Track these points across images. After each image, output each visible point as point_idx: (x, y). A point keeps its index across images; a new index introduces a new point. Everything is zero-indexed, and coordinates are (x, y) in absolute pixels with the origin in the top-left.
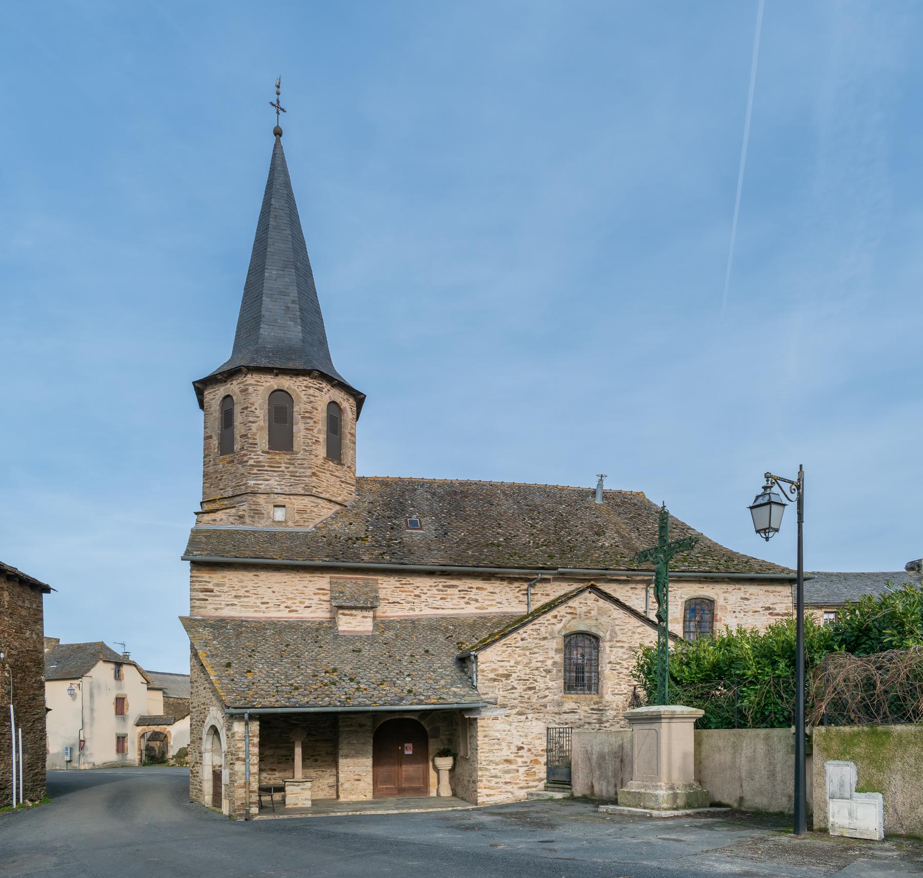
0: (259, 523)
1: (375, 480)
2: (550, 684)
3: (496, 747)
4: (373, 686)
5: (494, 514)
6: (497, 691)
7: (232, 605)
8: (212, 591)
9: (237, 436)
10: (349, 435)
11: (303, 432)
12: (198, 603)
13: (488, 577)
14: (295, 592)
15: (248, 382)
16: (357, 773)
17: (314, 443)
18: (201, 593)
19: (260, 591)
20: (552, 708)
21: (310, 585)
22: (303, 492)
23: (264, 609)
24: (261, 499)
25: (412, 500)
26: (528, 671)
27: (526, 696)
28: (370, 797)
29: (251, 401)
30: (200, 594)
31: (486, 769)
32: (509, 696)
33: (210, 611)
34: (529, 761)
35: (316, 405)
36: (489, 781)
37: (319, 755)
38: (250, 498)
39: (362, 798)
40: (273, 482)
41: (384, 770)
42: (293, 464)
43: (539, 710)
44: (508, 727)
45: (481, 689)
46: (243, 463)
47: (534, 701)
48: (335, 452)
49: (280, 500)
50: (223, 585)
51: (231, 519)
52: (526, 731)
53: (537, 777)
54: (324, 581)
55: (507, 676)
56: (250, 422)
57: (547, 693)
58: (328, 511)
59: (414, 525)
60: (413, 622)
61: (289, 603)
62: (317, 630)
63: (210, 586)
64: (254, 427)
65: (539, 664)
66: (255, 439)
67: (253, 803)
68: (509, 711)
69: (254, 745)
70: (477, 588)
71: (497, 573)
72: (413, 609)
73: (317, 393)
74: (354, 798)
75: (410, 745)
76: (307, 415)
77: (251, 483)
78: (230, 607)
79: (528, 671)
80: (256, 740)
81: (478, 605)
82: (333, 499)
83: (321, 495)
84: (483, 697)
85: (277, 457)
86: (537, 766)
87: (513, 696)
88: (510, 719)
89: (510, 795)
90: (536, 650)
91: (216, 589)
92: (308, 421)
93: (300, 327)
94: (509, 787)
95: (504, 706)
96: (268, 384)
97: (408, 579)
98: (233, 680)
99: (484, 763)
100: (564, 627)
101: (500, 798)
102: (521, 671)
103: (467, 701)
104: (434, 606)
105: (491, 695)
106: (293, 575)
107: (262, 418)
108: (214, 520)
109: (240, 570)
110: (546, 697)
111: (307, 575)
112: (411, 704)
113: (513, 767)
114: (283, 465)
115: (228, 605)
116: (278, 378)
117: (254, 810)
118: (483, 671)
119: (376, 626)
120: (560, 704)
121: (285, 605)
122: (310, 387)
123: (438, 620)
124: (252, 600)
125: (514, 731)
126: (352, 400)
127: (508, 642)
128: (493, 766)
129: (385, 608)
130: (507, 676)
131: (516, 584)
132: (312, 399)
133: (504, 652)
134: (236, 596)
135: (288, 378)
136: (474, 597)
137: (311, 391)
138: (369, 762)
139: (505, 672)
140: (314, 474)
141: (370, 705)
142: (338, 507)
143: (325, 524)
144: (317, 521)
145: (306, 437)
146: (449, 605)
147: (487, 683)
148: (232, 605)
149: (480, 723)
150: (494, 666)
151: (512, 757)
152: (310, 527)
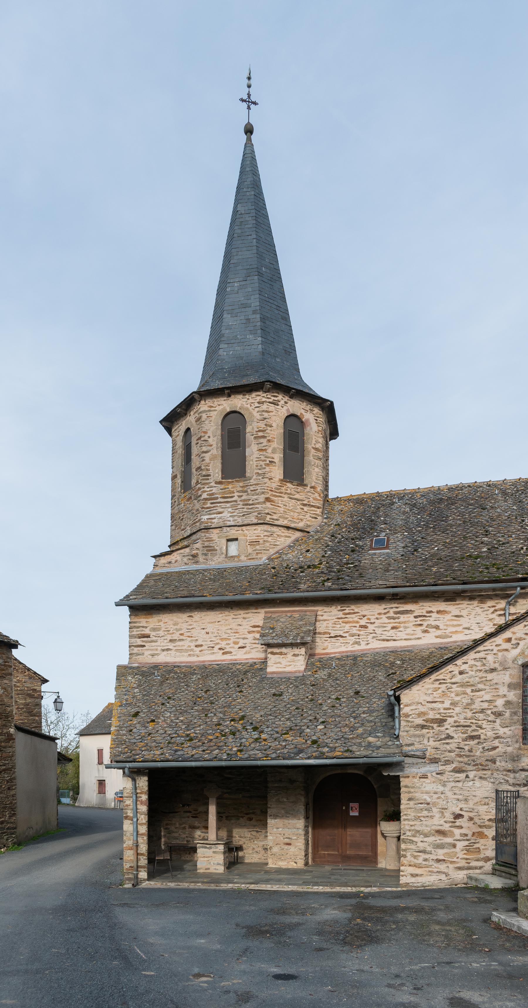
0: (212, 560)
1: (349, 499)
2: (502, 731)
3: (425, 813)
4: (276, 735)
5: (483, 519)
6: (425, 742)
7: (168, 650)
8: (148, 636)
9: (194, 470)
10: (313, 451)
11: (256, 454)
12: (136, 650)
13: (451, 597)
14: (229, 631)
15: (201, 409)
16: (286, 835)
17: (267, 465)
18: (139, 639)
19: (194, 633)
20: (503, 764)
21: (245, 623)
22: (255, 521)
23: (198, 652)
24: (214, 534)
25: (386, 516)
26: (469, 714)
27: (467, 748)
28: (300, 864)
29: (204, 430)
30: (138, 640)
31: (412, 842)
32: (443, 747)
33: (147, 658)
34: (470, 833)
35: (270, 422)
36: (415, 857)
37: (254, 813)
38: (203, 535)
39: (292, 865)
40: (226, 515)
41: (326, 834)
42: (246, 492)
43: (485, 766)
44: (441, 788)
45: (405, 739)
46: (198, 497)
47: (478, 754)
48: (294, 472)
49: (233, 532)
50: (159, 629)
51: (185, 560)
52: (466, 793)
53: (482, 856)
54: (257, 617)
55: (441, 722)
56: (204, 452)
57: (496, 743)
58: (284, 539)
59: (381, 544)
60: (355, 658)
61: (223, 644)
62: (245, 673)
63: (147, 631)
64: (207, 456)
65: (485, 705)
66: (208, 470)
67: (142, 867)
68: (441, 768)
69: (142, 803)
70: (438, 612)
71: (464, 591)
72: (358, 643)
73: (272, 407)
74: (283, 864)
75: (355, 805)
76: (260, 434)
77: (205, 518)
78: (165, 653)
79: (469, 714)
80: (144, 797)
81: (439, 633)
82: (293, 525)
83: (276, 523)
84: (406, 749)
85: (230, 486)
86: (482, 841)
87: (448, 747)
88: (444, 778)
89: (443, 877)
90: (481, 686)
91: (152, 634)
92: (262, 440)
93: (260, 339)
94: (442, 867)
95: (435, 761)
96: (221, 407)
97: (353, 607)
98: (131, 731)
99: (408, 833)
100: (522, 653)
101: (429, 879)
102: (459, 715)
103: (379, 756)
104: (384, 637)
105: (417, 746)
106: (227, 613)
107: (215, 446)
108: (170, 563)
109: (175, 612)
110: (495, 748)
111: (241, 612)
112: (309, 758)
113: (449, 840)
114: (236, 494)
115: (163, 650)
116: (230, 399)
117: (143, 875)
118: (407, 716)
119: (309, 665)
120: (515, 758)
121: (219, 646)
122: (263, 403)
123: (386, 654)
124: (186, 644)
125: (449, 794)
126: (317, 410)
127: (441, 677)
128: (421, 838)
129: (326, 644)
130: (441, 722)
131: (490, 603)
132: (266, 415)
133: (436, 690)
134: (171, 641)
135: (241, 396)
136: (434, 623)
137: (264, 407)
138: (300, 823)
139: (438, 716)
140: (268, 499)
141: (259, 759)
142: (298, 534)
143: (280, 553)
144: (272, 551)
145: (259, 459)
146: (402, 635)
147: (412, 731)
148: (168, 650)
149: (404, 782)
150: (422, 709)
151: (446, 827)
152: (263, 559)
